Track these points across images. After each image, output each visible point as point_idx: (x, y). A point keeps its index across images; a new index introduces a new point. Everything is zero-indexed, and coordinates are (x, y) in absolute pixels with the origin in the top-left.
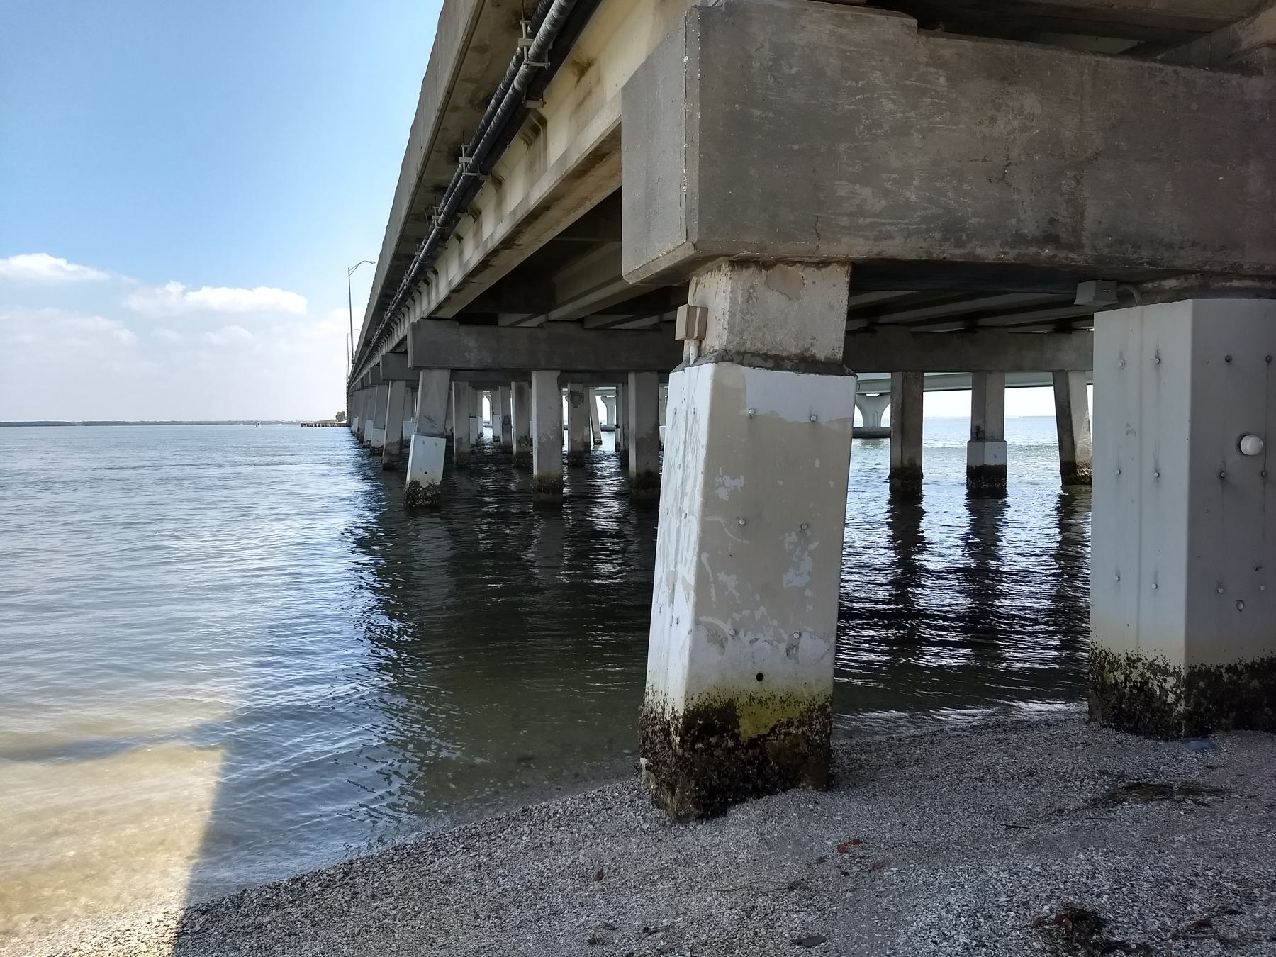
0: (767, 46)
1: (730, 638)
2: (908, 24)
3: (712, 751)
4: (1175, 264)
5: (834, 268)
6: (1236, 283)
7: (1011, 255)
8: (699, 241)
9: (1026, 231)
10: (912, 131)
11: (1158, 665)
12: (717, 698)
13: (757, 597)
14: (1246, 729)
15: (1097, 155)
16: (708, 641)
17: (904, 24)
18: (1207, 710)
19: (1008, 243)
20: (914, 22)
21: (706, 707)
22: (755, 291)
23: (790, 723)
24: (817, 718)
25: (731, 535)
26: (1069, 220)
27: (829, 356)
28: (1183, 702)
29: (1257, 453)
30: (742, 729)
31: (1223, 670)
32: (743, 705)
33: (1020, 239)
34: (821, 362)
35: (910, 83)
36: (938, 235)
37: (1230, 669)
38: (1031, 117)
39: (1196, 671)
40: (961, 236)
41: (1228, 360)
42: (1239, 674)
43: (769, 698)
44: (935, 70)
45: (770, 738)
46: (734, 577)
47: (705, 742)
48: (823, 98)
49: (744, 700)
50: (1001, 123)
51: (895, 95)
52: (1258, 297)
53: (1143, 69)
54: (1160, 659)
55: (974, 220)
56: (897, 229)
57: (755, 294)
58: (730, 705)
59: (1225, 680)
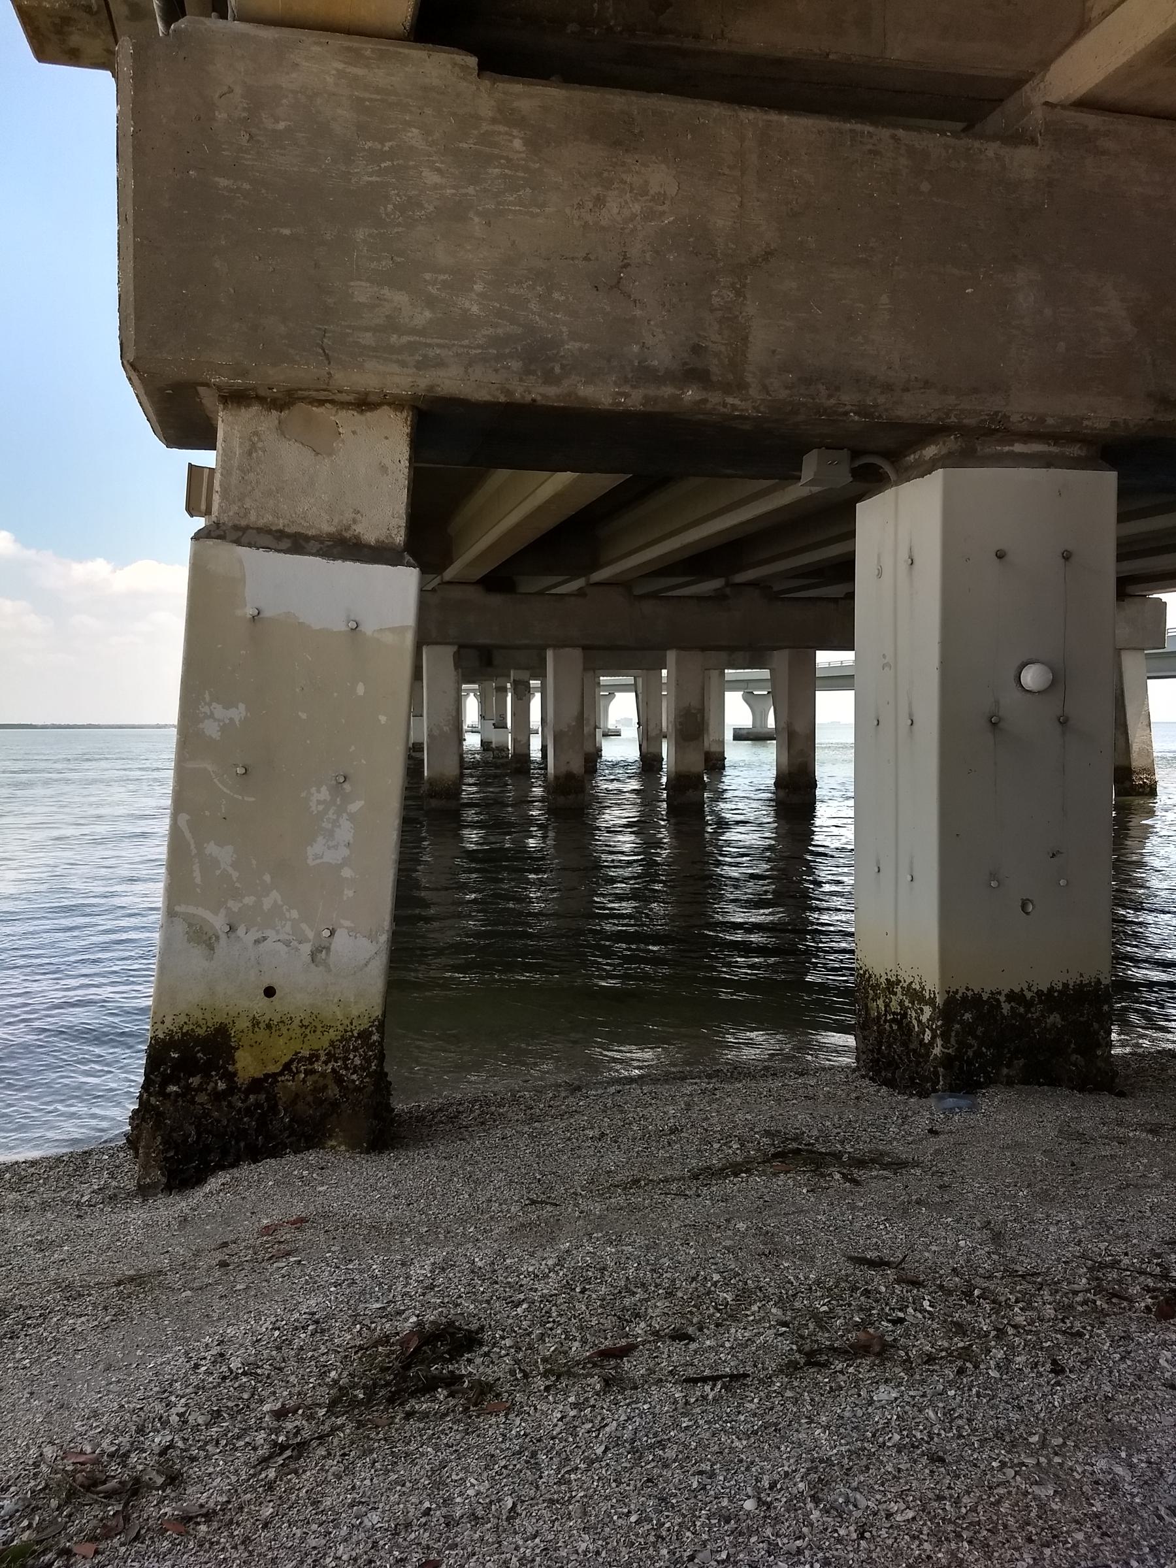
0: (238, 90)
1: (223, 937)
2: (463, 63)
3: (193, 1097)
4: (899, 413)
5: (385, 413)
6: (1018, 448)
7: (635, 399)
8: (137, 358)
9: (656, 363)
10: (471, 214)
11: (915, 989)
12: (201, 1022)
13: (267, 878)
14: (1040, 1085)
15: (768, 254)
16: (189, 941)
17: (455, 64)
18: (979, 1054)
19: (626, 381)
20: (472, 61)
21: (184, 1035)
22: (260, 440)
23: (314, 1057)
24: (356, 1049)
25: (225, 790)
26: (723, 348)
27: (382, 538)
28: (939, 1042)
29: (1047, 685)
30: (239, 1065)
31: (1002, 998)
32: (243, 1032)
33: (645, 374)
34: (370, 547)
35: (465, 145)
36: (516, 365)
37: (1012, 997)
38: (660, 198)
39: (958, 997)
40: (553, 369)
41: (1000, 555)
42: (1029, 1004)
43: (282, 1022)
44: (506, 129)
45: (283, 1078)
46: (229, 849)
47: (183, 1083)
48: (328, 164)
49: (244, 1024)
50: (613, 206)
51: (442, 162)
52: (1048, 465)
53: (842, 133)
54: (917, 980)
55: (572, 346)
56: (451, 353)
57: (260, 445)
58: (222, 1031)
59: (1005, 1012)
